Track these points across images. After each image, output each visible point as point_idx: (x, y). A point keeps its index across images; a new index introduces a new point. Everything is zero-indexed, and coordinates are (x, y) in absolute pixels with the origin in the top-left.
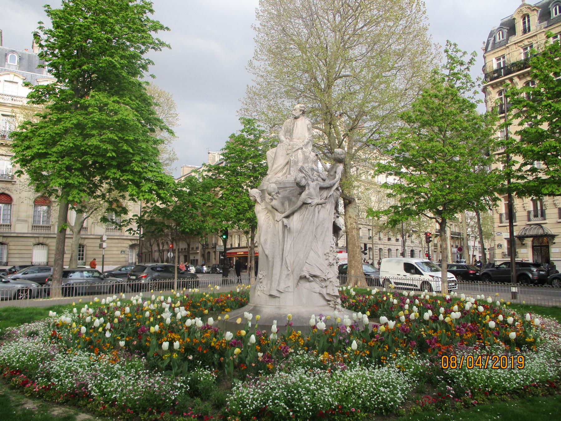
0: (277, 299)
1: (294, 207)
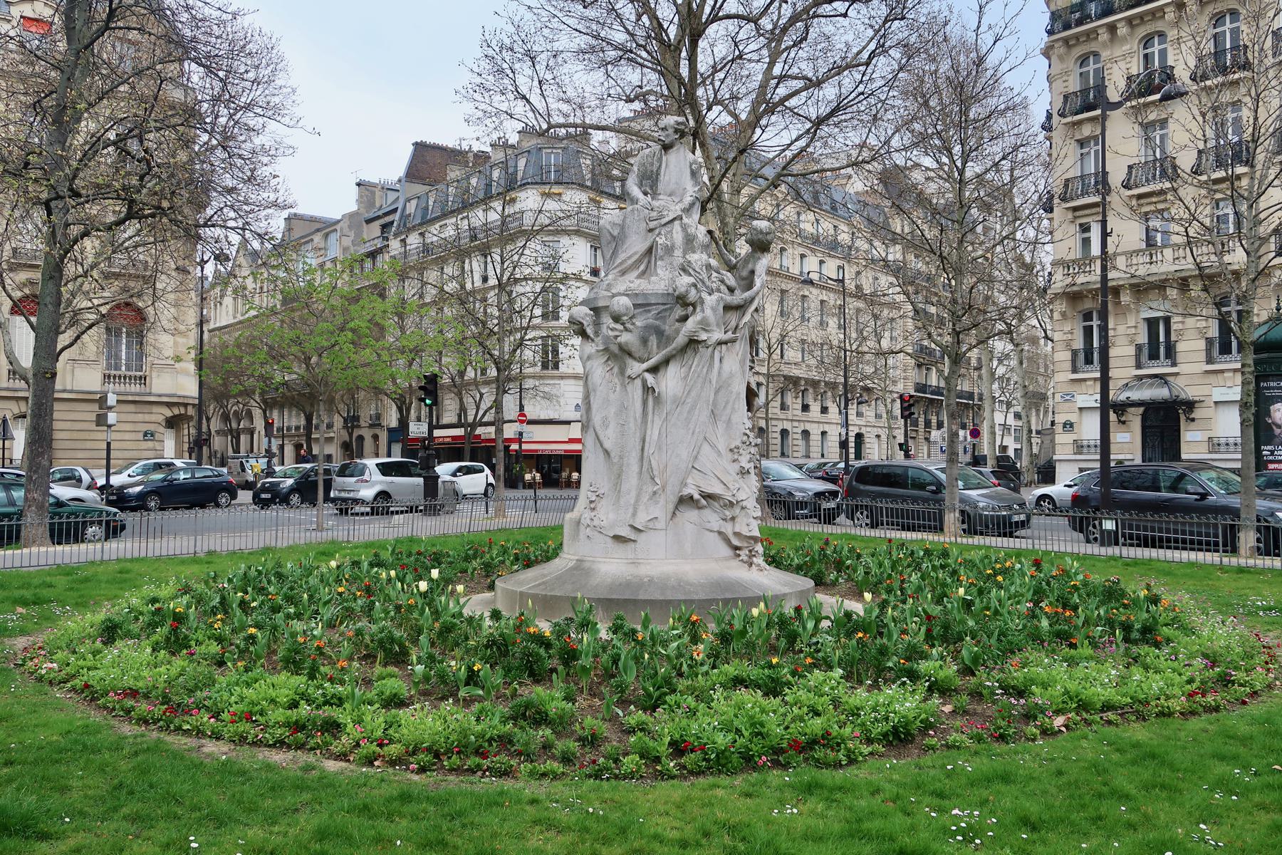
0: (632, 545)
1: (669, 349)
